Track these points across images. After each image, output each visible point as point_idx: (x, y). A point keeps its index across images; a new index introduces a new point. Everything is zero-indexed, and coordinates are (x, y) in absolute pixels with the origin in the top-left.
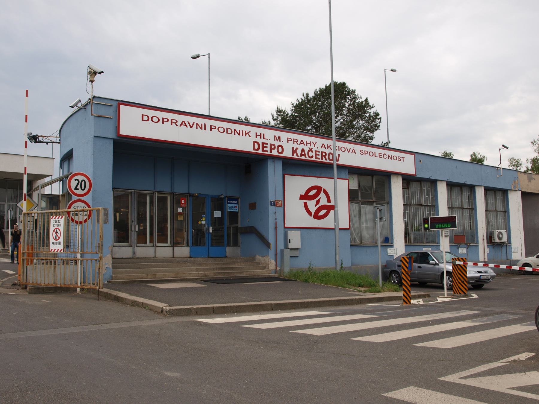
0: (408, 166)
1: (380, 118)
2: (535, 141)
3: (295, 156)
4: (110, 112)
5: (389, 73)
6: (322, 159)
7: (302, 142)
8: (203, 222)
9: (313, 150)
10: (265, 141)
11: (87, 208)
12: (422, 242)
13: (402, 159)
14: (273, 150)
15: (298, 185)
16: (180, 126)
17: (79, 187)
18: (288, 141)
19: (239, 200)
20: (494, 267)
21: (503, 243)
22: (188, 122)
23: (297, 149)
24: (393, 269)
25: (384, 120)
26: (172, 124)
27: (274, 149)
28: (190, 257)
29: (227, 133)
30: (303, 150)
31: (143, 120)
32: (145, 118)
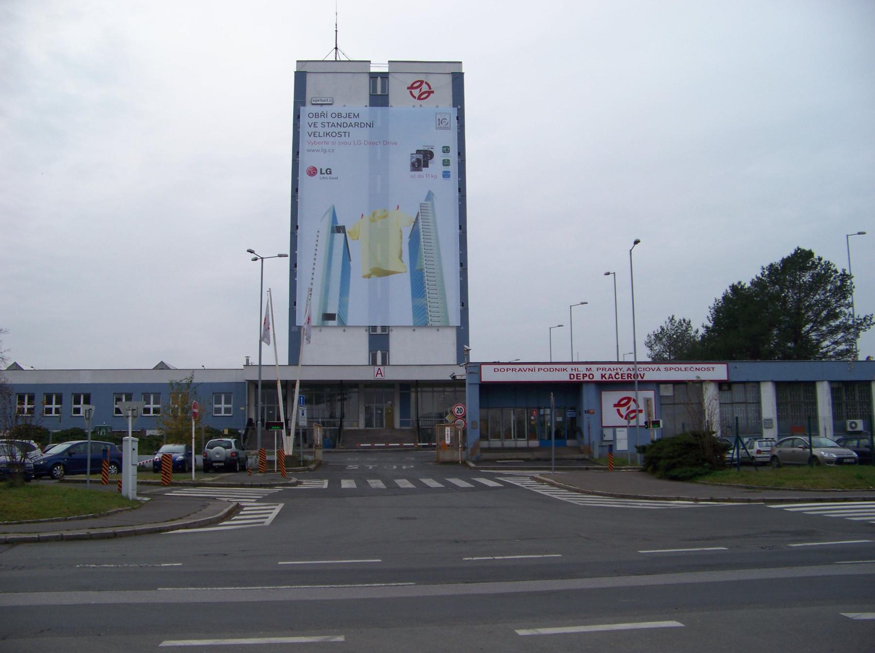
5: (855, 240)
15: (610, 398)
21: (859, 432)
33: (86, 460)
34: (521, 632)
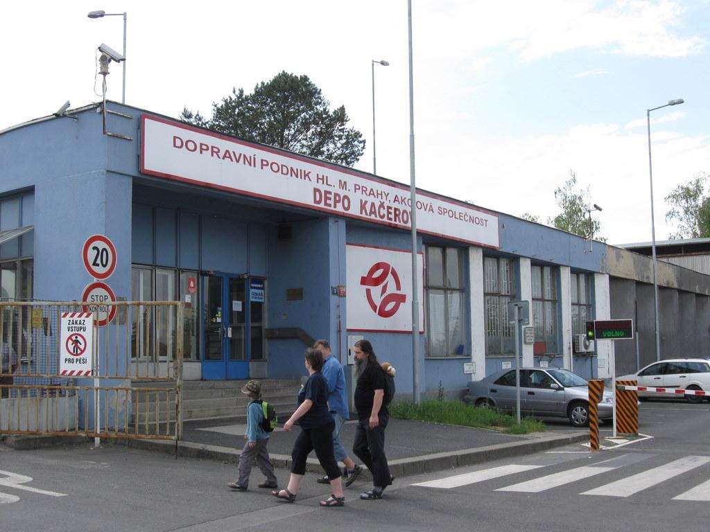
0: (489, 235)
1: (364, 142)
2: (560, 191)
3: (364, 215)
4: (128, 130)
5: (378, 67)
6: (395, 220)
7: (372, 193)
8: (219, 320)
9: (385, 205)
10: (328, 189)
11: (109, 301)
12: (500, 353)
13: (484, 222)
14: (337, 204)
15: (358, 260)
16: (223, 159)
17: (99, 261)
18: (356, 189)
19: (266, 283)
20: (674, 392)
22: (234, 152)
23: (366, 202)
24: (483, 396)
25: (369, 145)
26: (212, 155)
27: (339, 202)
28: (202, 380)
29: (282, 173)
30: (373, 204)
31: (175, 146)
32: (178, 143)
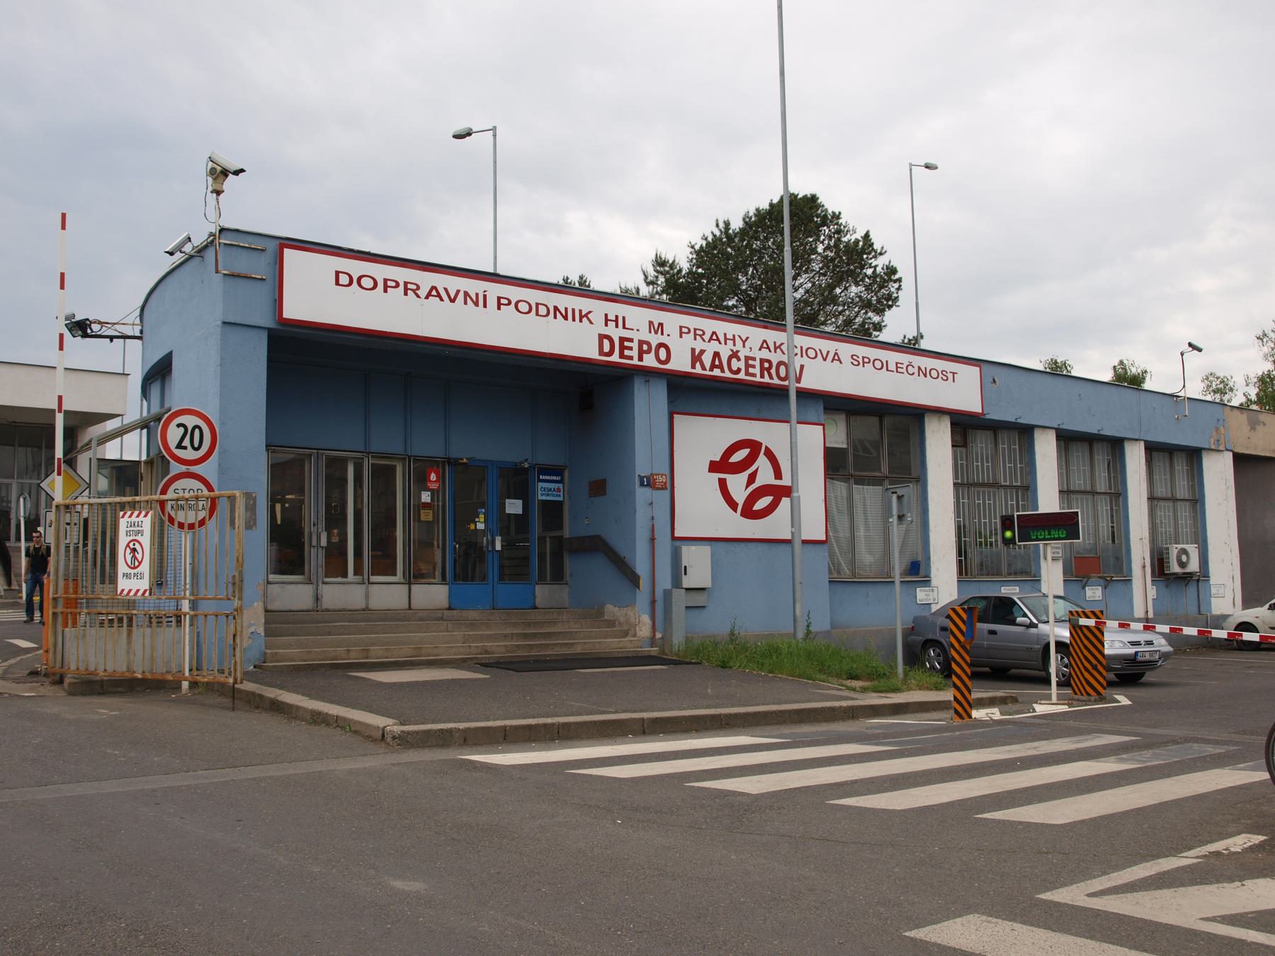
0: (964, 394)
1: (899, 280)
2: (1265, 335)
3: (698, 370)
4: (259, 266)
5: (920, 172)
6: (762, 376)
7: (714, 337)
8: (481, 526)
9: (741, 355)
10: (626, 334)
11: (206, 492)
12: (999, 574)
13: (950, 376)
14: (645, 356)
15: (704, 437)
16: (427, 298)
17: (186, 442)
18: (681, 333)
19: (566, 474)
20: (1168, 631)
21: (1191, 575)
22: (446, 290)
23: (702, 352)
24: (930, 637)
25: (907, 284)
26: (406, 294)
27: (649, 351)
28: (450, 608)
29: (537, 314)
30: (716, 355)
31: (337, 283)
32: (344, 279)
33: (51, 428)
34: (398, 884)
